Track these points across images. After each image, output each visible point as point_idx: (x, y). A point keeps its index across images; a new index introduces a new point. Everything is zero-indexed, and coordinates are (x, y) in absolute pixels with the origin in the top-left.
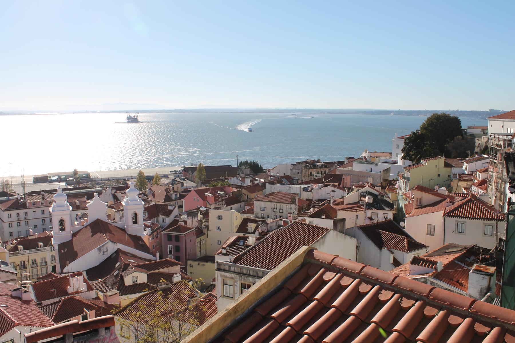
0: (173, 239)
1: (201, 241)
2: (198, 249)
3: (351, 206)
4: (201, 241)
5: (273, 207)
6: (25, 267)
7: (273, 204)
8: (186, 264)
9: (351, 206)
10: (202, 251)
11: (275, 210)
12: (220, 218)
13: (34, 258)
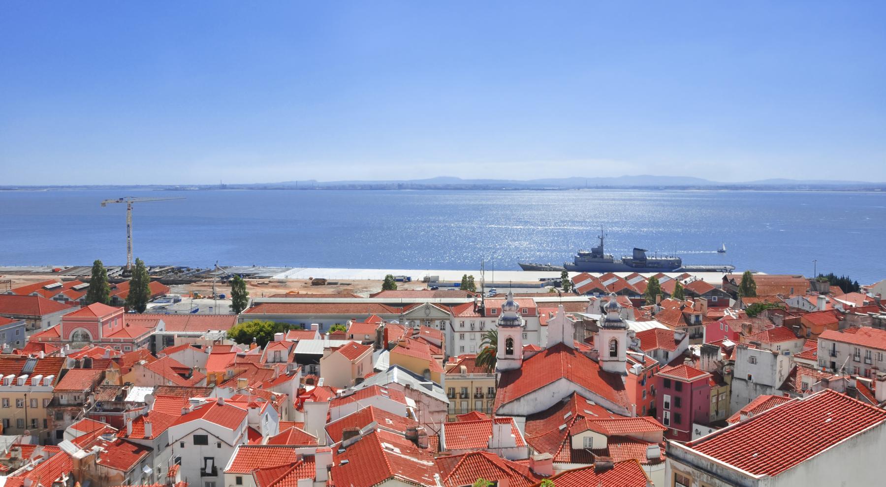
0: (673, 385)
1: (718, 395)
2: (713, 408)
3: (615, 324)
4: (718, 395)
5: (853, 352)
6: (467, 397)
7: (852, 347)
8: (691, 429)
9: (615, 324)
10: (720, 411)
11: (857, 359)
12: (753, 361)
13: (478, 385)
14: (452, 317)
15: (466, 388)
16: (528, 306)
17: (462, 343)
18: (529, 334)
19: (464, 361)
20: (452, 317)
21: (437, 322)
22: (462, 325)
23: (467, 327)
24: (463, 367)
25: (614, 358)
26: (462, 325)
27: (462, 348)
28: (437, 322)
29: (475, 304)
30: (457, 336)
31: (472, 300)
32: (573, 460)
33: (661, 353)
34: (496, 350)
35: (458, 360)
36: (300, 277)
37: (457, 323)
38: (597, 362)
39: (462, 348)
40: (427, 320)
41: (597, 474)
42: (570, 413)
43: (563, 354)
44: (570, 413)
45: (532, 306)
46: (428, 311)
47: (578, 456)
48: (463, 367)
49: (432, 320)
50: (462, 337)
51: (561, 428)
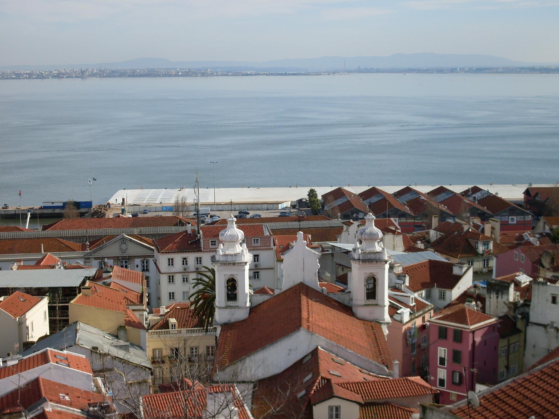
0: (450, 335)
10: (511, 366)
13: (194, 344)
17: (172, 288)
19: (174, 312)
21: (138, 261)
24: (173, 321)
25: (372, 302)
27: (172, 296)
28: (138, 261)
36: (235, 200)
39: (172, 296)
40: (124, 258)
44: (310, 376)
46: (124, 246)
48: (173, 321)
49: (130, 258)
50: (171, 279)
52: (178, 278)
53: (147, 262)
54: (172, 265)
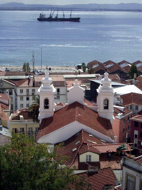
14: (15, 87)
15: (23, 129)
16: (60, 80)
18: (61, 97)
20: (15, 87)
21: (8, 91)
22: (22, 91)
23: (25, 93)
24: (21, 116)
26: (22, 91)
27: (22, 105)
28: (8, 91)
29: (29, 80)
30: (19, 98)
31: (28, 77)
32: (80, 169)
33: (134, 107)
34: (38, 107)
35: (19, 112)
37: (18, 90)
38: (97, 113)
39: (22, 105)
41: (88, 177)
42: (79, 142)
43: (77, 108)
44: (79, 142)
45: (63, 80)
47: (82, 166)
48: (21, 116)
49: (5, 89)
50: (22, 98)
51: (74, 150)
52: (25, 98)
53: (11, 91)
54: (22, 92)
